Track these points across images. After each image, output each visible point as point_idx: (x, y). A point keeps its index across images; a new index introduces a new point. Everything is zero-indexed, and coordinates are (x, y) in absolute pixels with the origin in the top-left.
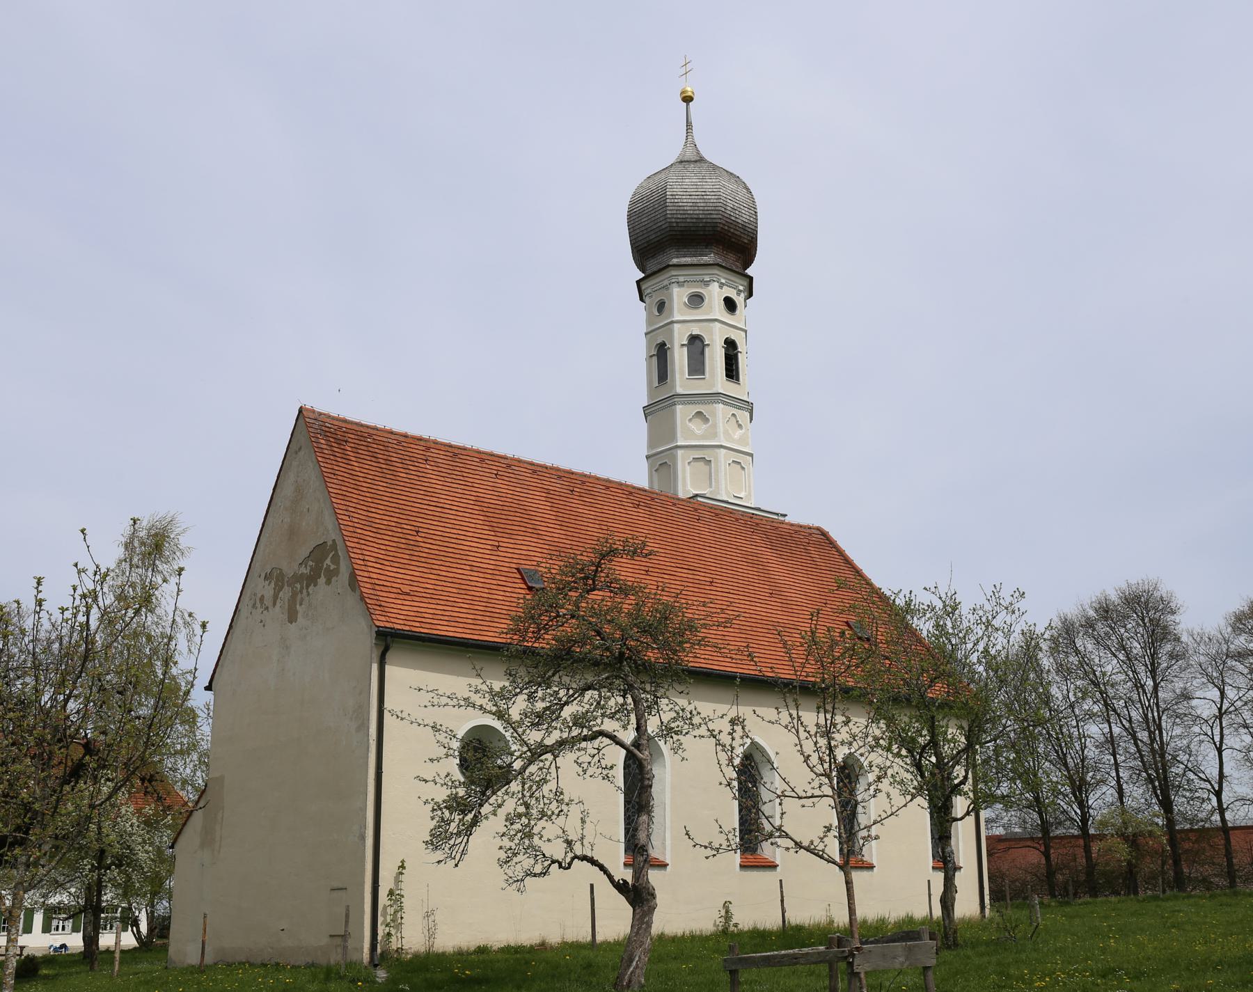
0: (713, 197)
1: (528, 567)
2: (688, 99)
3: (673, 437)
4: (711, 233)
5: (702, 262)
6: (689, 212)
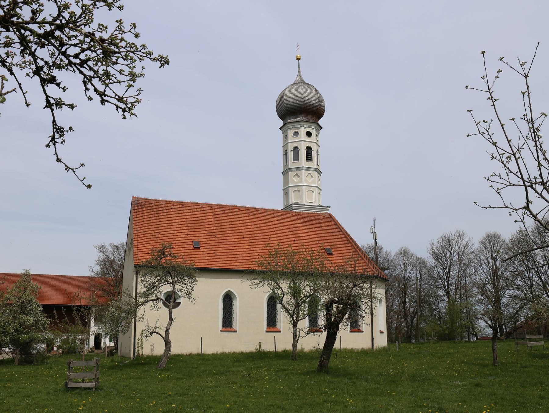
1: (197, 241)
2: (298, 59)
3: (288, 184)
5: (298, 120)
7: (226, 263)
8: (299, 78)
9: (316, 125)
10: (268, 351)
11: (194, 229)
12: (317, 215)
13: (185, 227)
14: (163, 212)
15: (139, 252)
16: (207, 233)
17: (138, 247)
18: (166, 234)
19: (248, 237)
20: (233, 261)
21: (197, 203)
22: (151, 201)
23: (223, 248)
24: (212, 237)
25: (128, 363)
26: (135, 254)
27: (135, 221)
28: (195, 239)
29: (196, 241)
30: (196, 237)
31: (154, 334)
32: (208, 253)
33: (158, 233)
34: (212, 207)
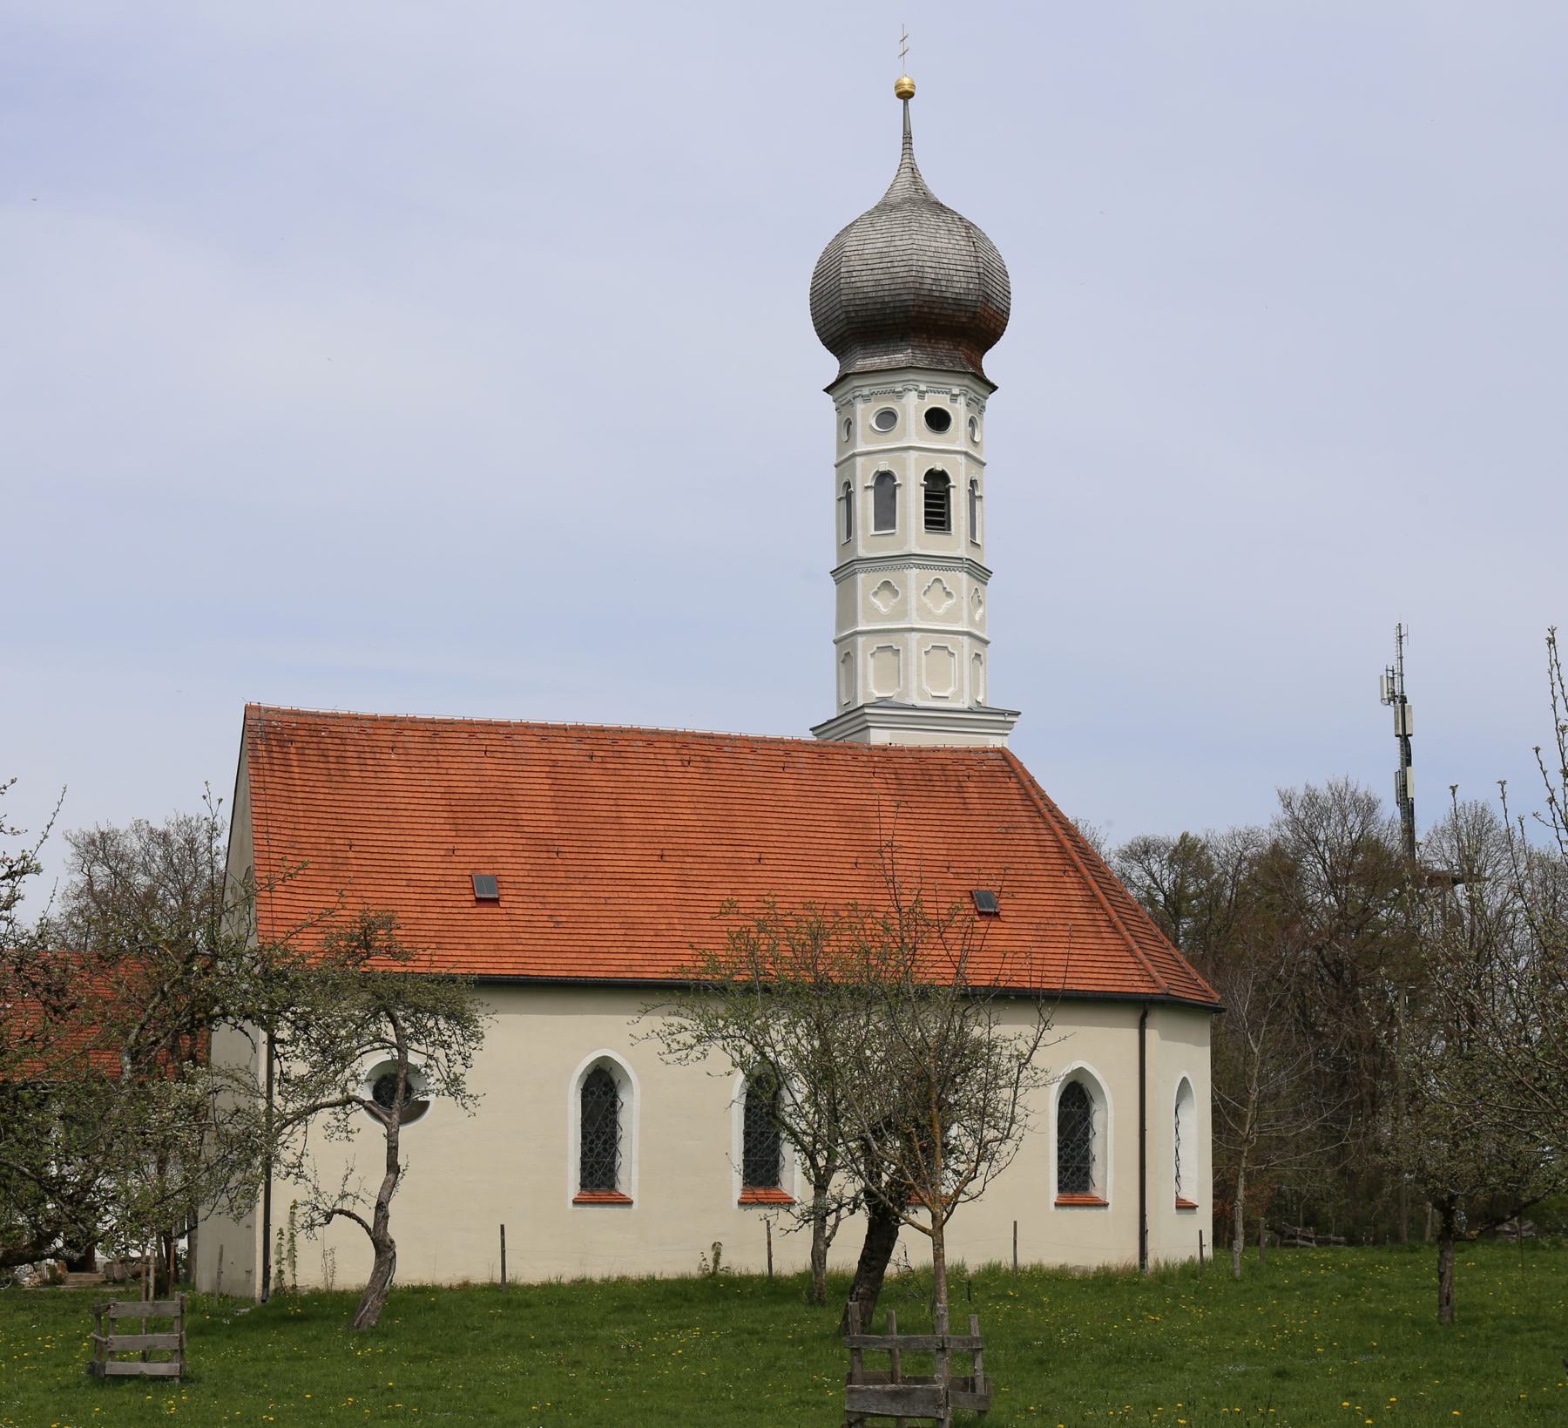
0: (903, 269)
1: (487, 872)
2: (905, 96)
3: (854, 622)
4: (904, 320)
5: (894, 365)
6: (870, 295)
7: (593, 956)
8: (906, 176)
9: (966, 382)
10: (744, 1273)
11: (476, 828)
12: (955, 756)
13: (442, 821)
14: (362, 761)
15: (279, 922)
16: (524, 841)
17: (274, 901)
18: (376, 850)
19: (680, 853)
20: (620, 950)
21: (489, 724)
22: (318, 721)
23: (585, 900)
24: (545, 855)
25: (244, 1316)
26: (264, 928)
27: (258, 804)
28: (482, 866)
29: (483, 872)
30: (485, 860)
31: (336, 1216)
32: (527, 918)
33: (342, 848)
34: (544, 739)
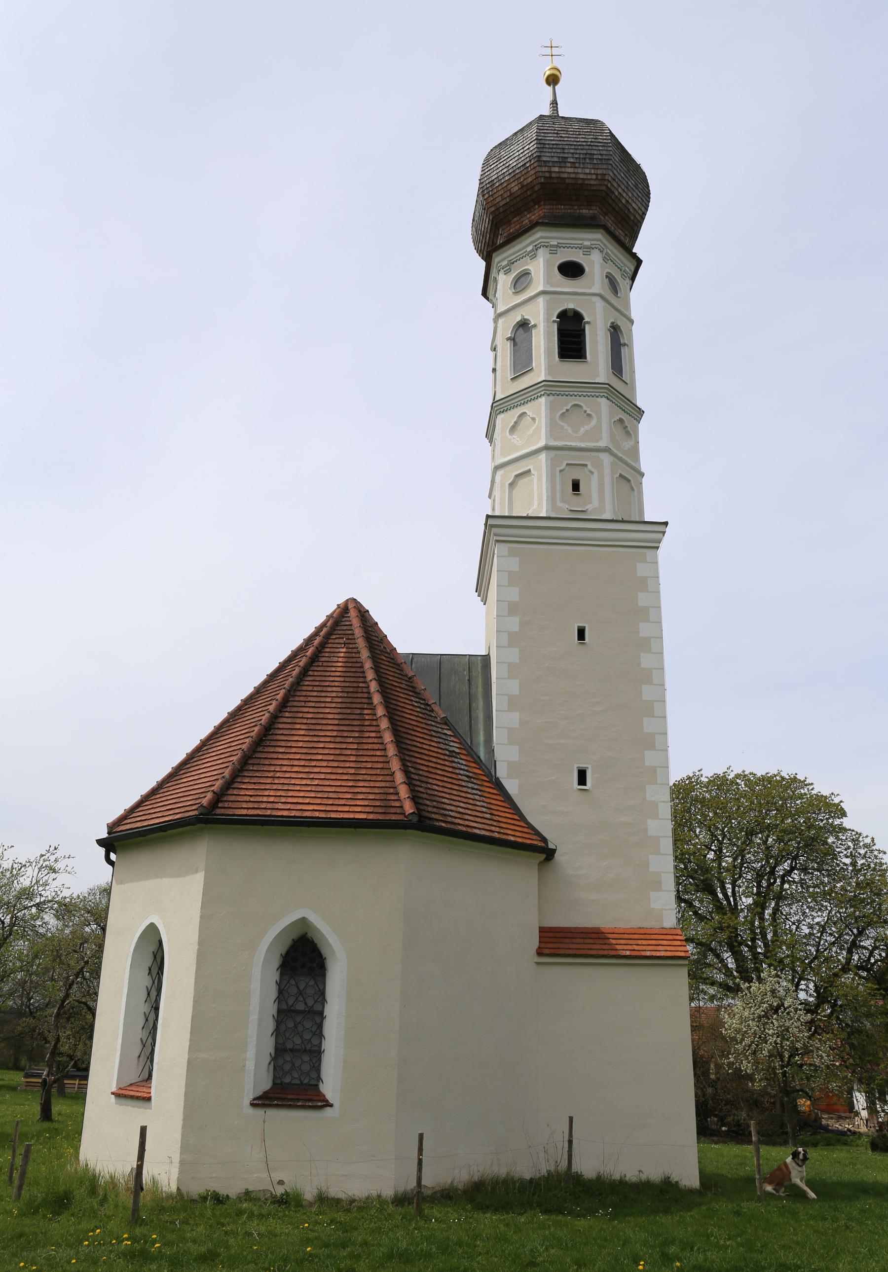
2: (553, 80)
